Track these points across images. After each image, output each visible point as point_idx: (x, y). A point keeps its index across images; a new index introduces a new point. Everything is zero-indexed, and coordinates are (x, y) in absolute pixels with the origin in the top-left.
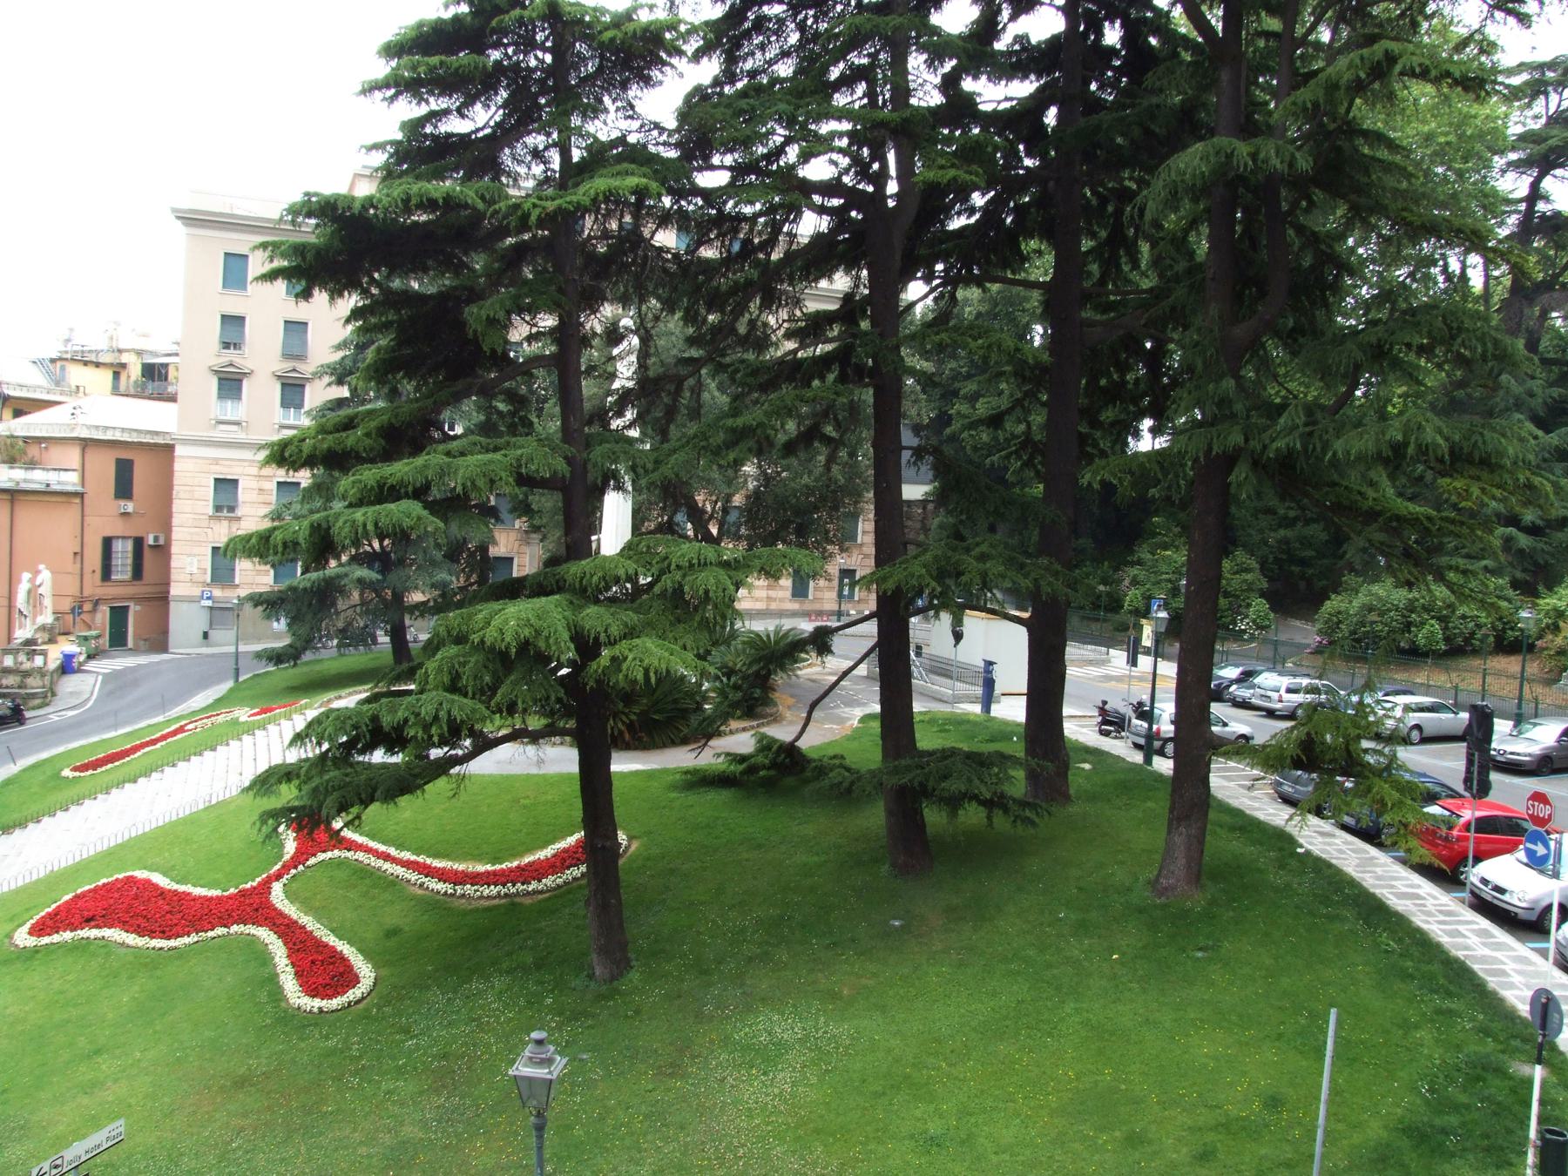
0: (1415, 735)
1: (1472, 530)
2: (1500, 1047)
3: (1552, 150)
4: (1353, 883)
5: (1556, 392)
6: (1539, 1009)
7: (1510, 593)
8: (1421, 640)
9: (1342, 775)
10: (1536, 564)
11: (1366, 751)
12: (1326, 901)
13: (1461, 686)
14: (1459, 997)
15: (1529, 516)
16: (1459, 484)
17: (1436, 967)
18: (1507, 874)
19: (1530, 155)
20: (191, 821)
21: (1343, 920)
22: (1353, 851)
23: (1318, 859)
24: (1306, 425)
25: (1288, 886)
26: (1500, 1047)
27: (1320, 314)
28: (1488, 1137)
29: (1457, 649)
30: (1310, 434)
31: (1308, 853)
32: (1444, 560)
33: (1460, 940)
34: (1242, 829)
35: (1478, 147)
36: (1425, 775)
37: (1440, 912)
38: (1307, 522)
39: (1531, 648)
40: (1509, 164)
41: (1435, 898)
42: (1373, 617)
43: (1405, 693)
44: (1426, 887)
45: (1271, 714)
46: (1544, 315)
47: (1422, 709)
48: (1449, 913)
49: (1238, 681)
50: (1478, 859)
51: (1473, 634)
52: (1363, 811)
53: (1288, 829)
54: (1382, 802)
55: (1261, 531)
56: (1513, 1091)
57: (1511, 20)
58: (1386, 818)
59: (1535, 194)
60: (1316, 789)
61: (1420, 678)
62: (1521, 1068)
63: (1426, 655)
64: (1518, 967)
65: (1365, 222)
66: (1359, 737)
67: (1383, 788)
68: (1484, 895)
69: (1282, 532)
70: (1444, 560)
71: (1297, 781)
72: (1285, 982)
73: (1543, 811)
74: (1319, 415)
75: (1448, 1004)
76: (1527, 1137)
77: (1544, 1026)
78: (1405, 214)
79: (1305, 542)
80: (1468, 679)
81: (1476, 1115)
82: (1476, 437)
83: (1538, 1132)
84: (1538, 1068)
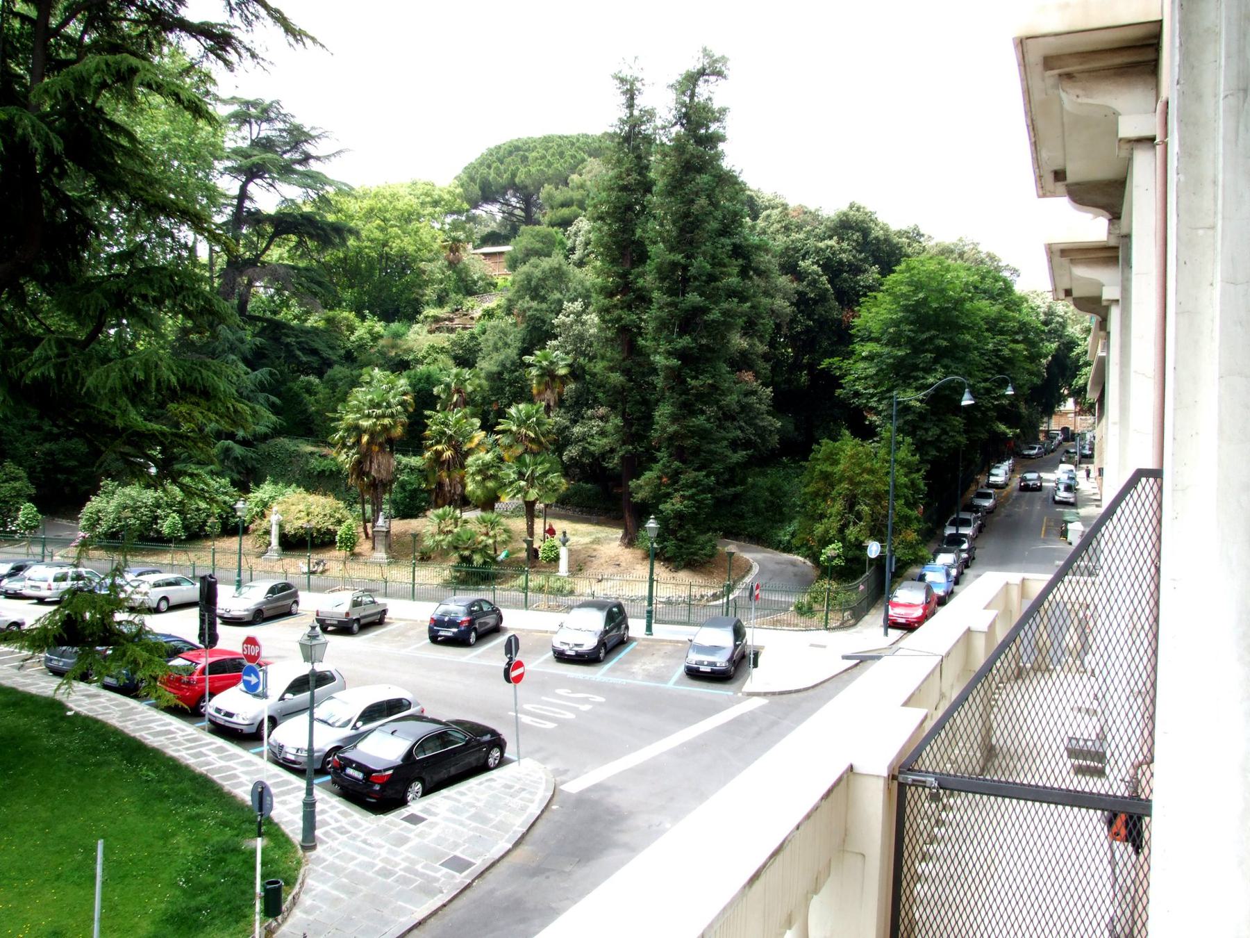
0: (164, 605)
1: (195, 443)
2: (235, 832)
3: (254, 165)
4: (116, 732)
5: (258, 340)
6: (257, 798)
7: (232, 490)
8: (166, 530)
9: (101, 645)
10: (247, 468)
11: (120, 623)
12: (95, 751)
13: (198, 563)
14: (203, 802)
15: (241, 433)
16: (184, 409)
17: (186, 784)
18: (234, 703)
19: (241, 166)
20: (776, 742)
21: (109, 764)
22: (117, 705)
23: (87, 718)
24: (58, 356)
25: (60, 745)
26: (235, 832)
27: (72, 265)
28: (229, 902)
29: (194, 535)
30: (63, 364)
31: (77, 714)
32: (177, 467)
33: (202, 759)
34: (15, 704)
35: (204, 152)
36: (170, 636)
37: (188, 740)
38: (69, 438)
39: (246, 531)
40: (226, 169)
41: (183, 730)
42: (127, 513)
43: (154, 572)
44: (175, 723)
45: (41, 601)
46: (250, 284)
47: (169, 584)
48: (195, 740)
49: (10, 575)
50: (213, 694)
51: (205, 522)
52: (121, 672)
53: (58, 697)
54: (135, 662)
55: (28, 445)
56: (245, 862)
57: (220, 63)
58: (139, 675)
59: (243, 195)
60: (79, 660)
61: (166, 559)
62: (247, 844)
63: (169, 541)
64: (245, 769)
65: (109, 194)
66: (113, 612)
67: (136, 651)
68: (218, 721)
69: (47, 445)
70: (177, 467)
71: (62, 655)
72: (62, 829)
73: (253, 651)
74: (69, 349)
75: (196, 810)
76: (255, 893)
77: (261, 809)
78: (142, 193)
79: (69, 454)
80: (200, 559)
81: (220, 889)
82: (196, 374)
83: (263, 886)
84: (259, 840)
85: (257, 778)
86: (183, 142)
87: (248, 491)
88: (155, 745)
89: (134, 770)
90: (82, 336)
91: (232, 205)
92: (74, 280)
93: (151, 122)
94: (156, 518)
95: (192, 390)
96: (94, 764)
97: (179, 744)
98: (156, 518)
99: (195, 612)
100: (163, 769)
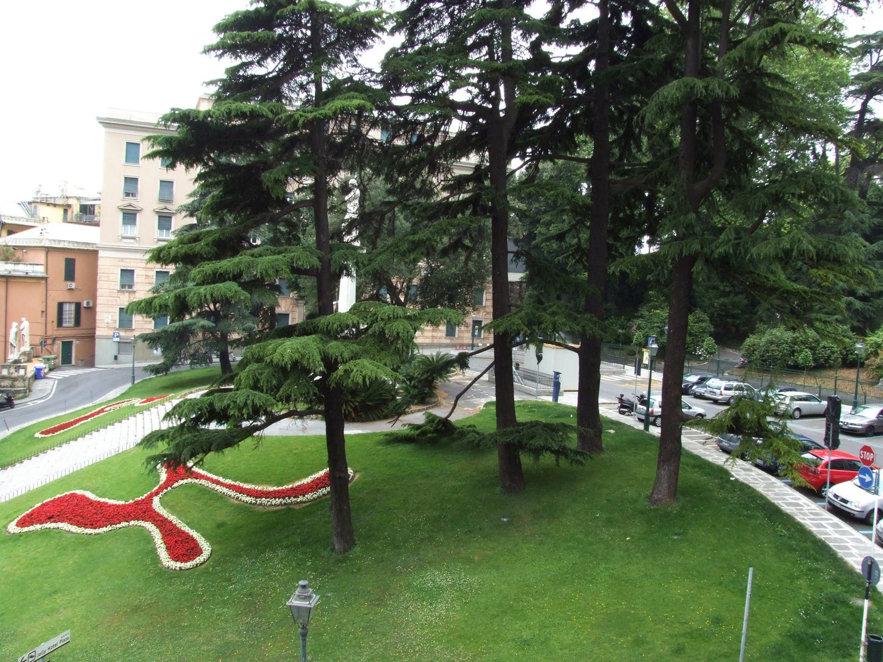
0: (797, 414)
1: (829, 299)
2: (845, 589)
3: (874, 84)
4: (762, 497)
5: (876, 221)
6: (867, 568)
7: (851, 334)
8: (800, 360)
9: (756, 436)
10: (865, 318)
11: (769, 423)
12: (747, 507)
13: (823, 386)
14: (822, 561)
15: (861, 291)
17: (809, 545)
18: (849, 492)
19: (862, 88)
22: (762, 479)
23: (743, 484)
24: (735, 239)
25: (725, 499)
26: (845, 589)
28: (838, 640)
29: (821, 366)
30: (738, 244)
31: (737, 480)
33: (822, 529)
34: (699, 467)
35: (832, 82)
36: (802, 436)
38: (736, 294)
39: (862, 365)
40: (850, 92)
41: (808, 505)
42: (773, 347)
43: (791, 390)
44: (803, 499)
45: (716, 402)
46: (870, 177)
47: (801, 399)
48: (816, 514)
49: (697, 383)
50: (832, 484)
51: (829, 357)
52: (768, 457)
53: (726, 467)
54: (778, 452)
55: (710, 299)
56: (852, 614)
57: (851, 11)
58: (781, 461)
59: (864, 109)
60: (741, 444)
62: (857, 602)
63: (803, 369)
66: (765, 415)
67: (779, 444)
68: (835, 504)
70: (813, 315)
71: (730, 440)
73: (869, 456)
74: (743, 234)
75: (815, 565)
76: (860, 640)
78: (791, 120)
79: (735, 305)
80: (827, 382)
81: (831, 628)
83: (866, 637)
84: (866, 601)
85: (866, 553)
86: (817, 78)
87: (865, 335)
88: (788, 512)
89: (773, 526)
90: (748, 225)
91: (855, 119)
92: (745, 188)
93: (797, 66)
94: (793, 352)
95: (827, 259)
96: (745, 516)
97: (805, 514)
98: (793, 352)
99: (823, 420)
100: (793, 530)
